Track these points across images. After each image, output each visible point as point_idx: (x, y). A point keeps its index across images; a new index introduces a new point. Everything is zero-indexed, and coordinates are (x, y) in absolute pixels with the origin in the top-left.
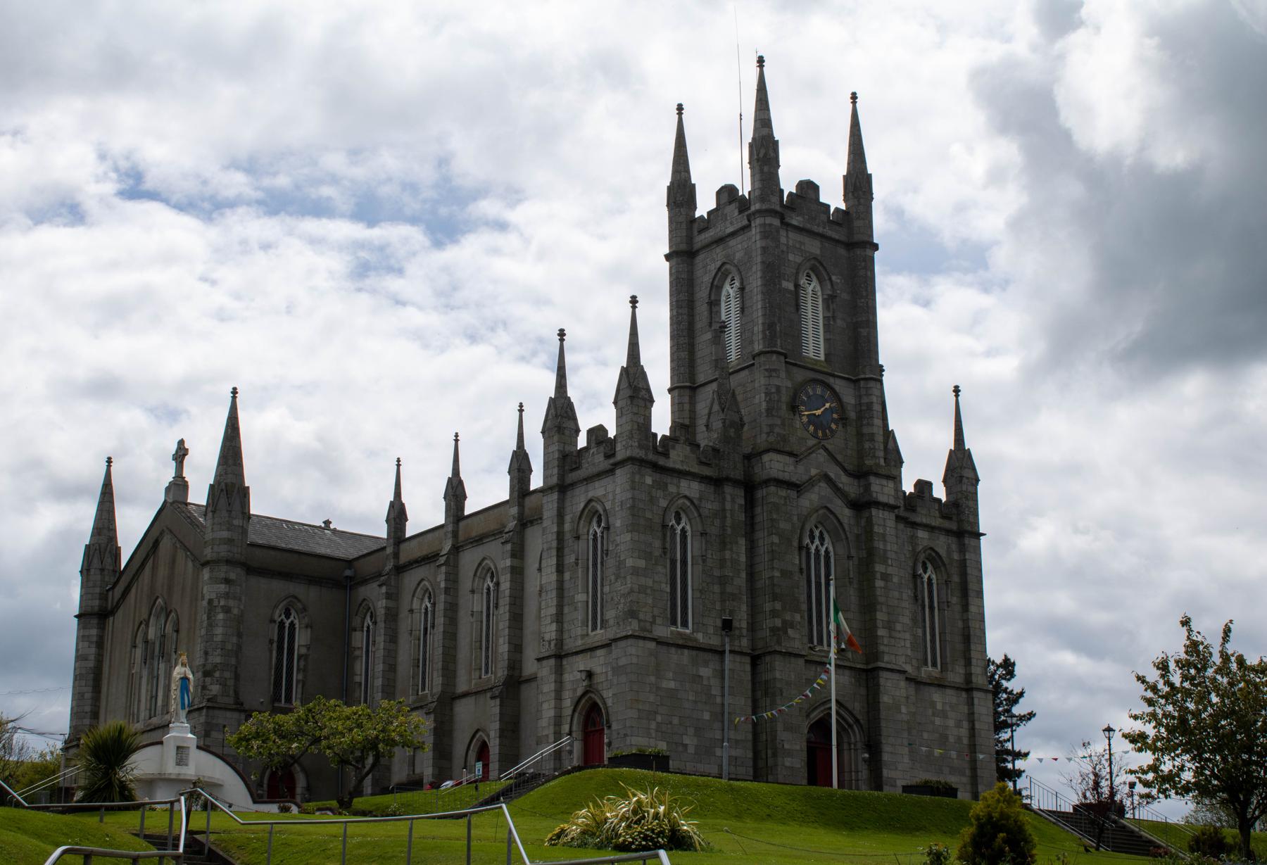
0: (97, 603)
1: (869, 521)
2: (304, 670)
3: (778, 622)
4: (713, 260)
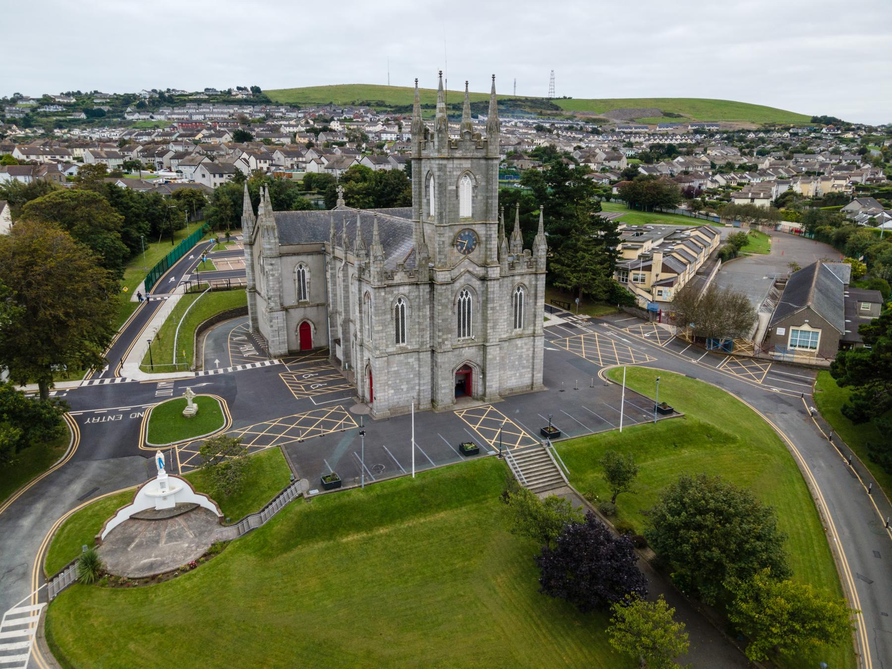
2: (309, 288)
3: (440, 340)
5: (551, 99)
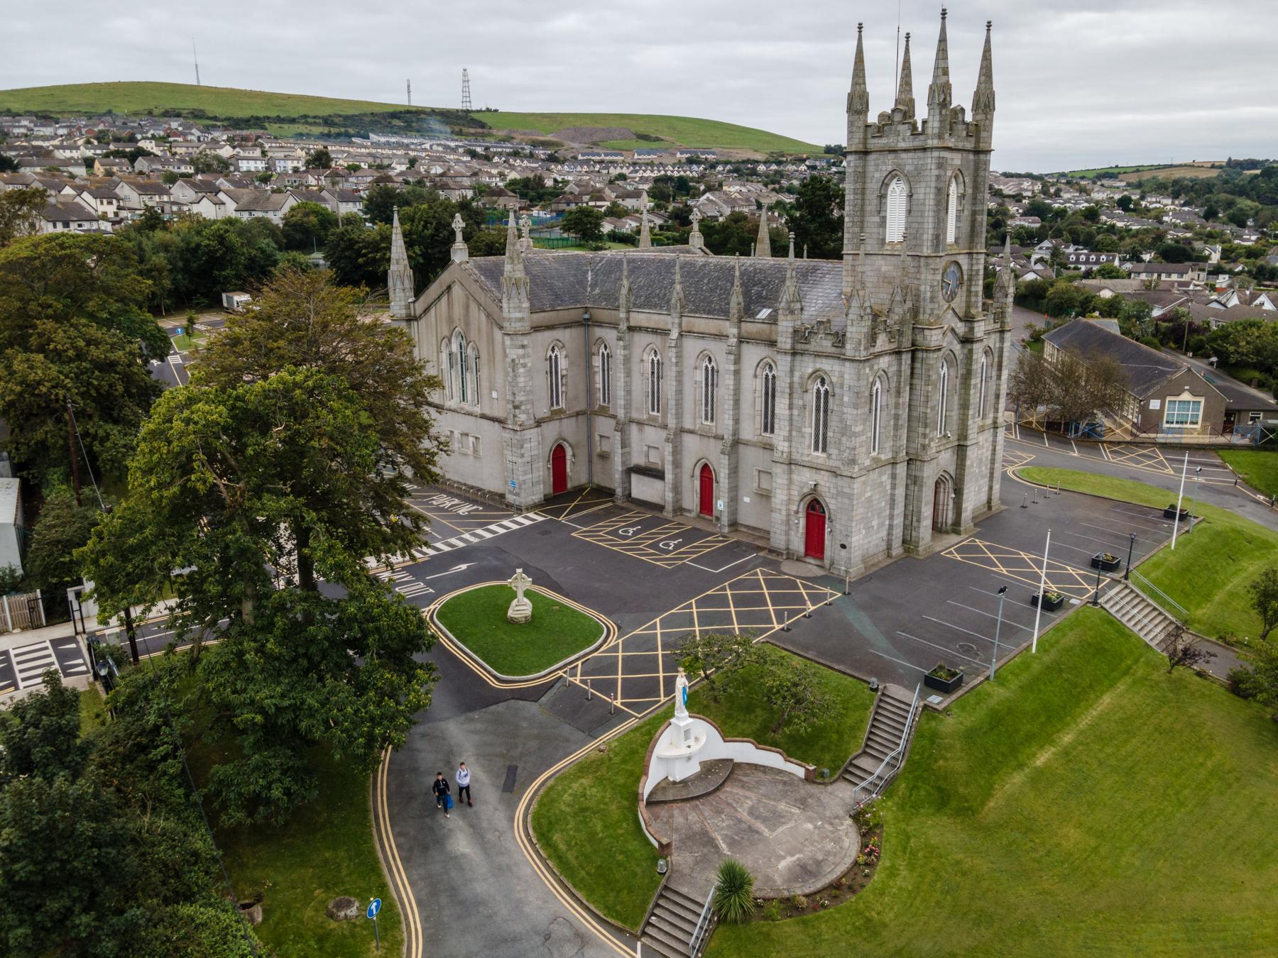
0: (404, 312)
1: (971, 351)
4: (885, 163)
5: (468, 111)
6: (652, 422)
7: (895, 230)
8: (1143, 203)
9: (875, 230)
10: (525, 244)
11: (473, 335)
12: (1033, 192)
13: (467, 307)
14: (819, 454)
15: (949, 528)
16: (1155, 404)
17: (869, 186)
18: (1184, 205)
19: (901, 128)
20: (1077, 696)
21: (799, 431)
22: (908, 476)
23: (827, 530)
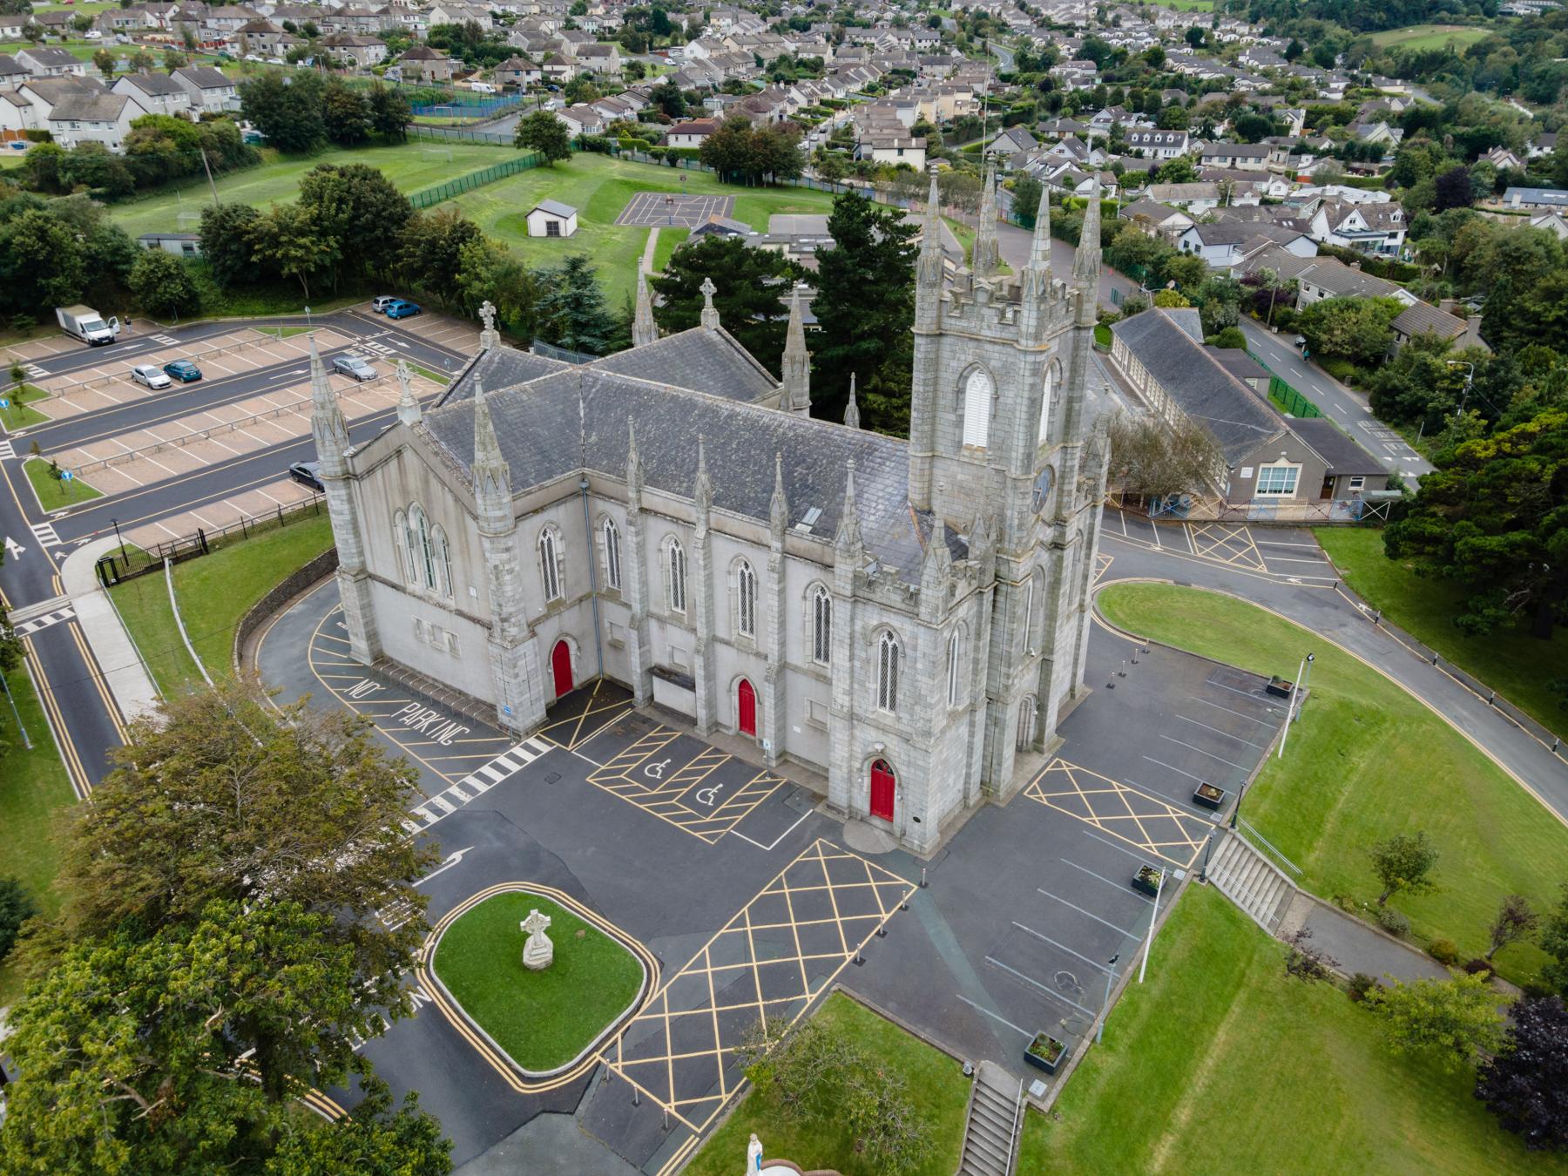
0: (339, 469)
1: (1061, 559)
6: (676, 620)
7: (976, 431)
8: (1216, 33)
9: (951, 430)
10: (490, 340)
11: (438, 515)
12: (1087, 18)
13: (426, 482)
14: (886, 711)
15: (1030, 746)
16: (1247, 472)
17: (943, 374)
18: (1263, 35)
19: (985, 311)
20: (1189, 1041)
21: (862, 685)
22: (989, 716)
23: (897, 798)
